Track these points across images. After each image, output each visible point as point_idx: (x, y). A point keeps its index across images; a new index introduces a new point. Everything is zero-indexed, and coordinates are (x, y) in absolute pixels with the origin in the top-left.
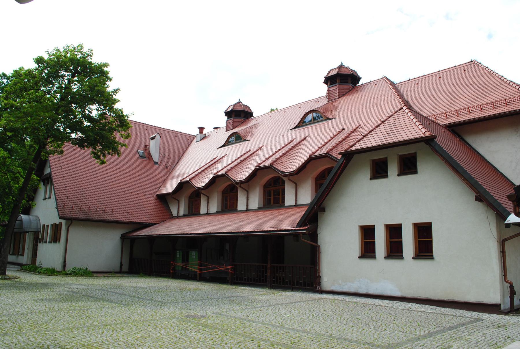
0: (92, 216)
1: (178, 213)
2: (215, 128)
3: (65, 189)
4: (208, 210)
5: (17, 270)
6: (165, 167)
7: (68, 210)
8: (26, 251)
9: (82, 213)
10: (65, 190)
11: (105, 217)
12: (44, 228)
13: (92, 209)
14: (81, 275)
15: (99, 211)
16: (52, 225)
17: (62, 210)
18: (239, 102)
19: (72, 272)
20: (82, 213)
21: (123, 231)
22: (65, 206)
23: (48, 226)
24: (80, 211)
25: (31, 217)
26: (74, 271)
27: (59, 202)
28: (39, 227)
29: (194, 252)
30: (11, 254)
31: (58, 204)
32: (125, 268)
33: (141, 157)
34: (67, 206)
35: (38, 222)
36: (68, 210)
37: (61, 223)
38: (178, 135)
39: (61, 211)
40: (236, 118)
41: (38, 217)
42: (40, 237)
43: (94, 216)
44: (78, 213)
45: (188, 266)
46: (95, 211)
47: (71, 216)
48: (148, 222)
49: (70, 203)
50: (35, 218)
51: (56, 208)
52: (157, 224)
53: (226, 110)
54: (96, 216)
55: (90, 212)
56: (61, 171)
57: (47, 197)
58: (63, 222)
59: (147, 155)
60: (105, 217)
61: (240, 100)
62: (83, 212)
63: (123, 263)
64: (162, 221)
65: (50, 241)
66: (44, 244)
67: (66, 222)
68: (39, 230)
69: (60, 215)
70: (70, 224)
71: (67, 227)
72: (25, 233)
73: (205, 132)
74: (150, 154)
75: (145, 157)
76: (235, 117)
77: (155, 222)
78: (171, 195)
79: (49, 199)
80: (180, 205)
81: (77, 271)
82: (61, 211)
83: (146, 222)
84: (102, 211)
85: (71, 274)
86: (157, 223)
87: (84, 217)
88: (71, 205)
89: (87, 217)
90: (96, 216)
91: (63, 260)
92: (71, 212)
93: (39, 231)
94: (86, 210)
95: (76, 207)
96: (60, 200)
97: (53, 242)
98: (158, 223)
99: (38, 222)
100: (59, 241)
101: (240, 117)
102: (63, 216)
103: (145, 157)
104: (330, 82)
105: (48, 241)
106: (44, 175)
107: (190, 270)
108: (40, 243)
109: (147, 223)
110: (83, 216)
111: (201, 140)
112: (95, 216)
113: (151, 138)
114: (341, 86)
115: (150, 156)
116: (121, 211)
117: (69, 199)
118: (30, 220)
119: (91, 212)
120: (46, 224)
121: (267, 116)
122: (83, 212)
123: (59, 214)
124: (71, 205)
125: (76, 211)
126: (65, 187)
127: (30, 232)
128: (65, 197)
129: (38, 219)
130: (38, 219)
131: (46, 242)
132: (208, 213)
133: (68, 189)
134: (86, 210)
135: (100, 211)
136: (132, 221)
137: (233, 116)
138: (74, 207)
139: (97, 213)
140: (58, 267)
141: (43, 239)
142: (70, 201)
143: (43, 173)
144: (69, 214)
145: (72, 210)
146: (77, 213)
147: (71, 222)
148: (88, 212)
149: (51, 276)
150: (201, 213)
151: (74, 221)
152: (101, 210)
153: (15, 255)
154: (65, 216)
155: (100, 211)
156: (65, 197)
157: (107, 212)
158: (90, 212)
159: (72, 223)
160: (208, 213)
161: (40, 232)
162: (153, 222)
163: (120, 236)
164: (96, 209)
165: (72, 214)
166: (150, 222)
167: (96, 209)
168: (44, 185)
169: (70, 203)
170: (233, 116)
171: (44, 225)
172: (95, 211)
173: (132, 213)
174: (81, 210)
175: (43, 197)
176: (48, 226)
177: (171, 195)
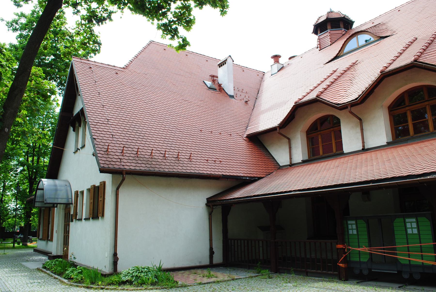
0: (157, 166)
1: (291, 159)
2: (290, 58)
3: (107, 123)
4: (363, 142)
5: (38, 269)
6: (243, 102)
7: (115, 157)
8: (55, 235)
9: (140, 162)
10: (108, 125)
11: (180, 168)
12: (77, 197)
13: (156, 154)
14: (153, 284)
15: (168, 158)
16: (89, 190)
17: (104, 156)
18: (331, 12)
19: (133, 276)
20: (140, 162)
21: (210, 193)
22: (109, 150)
23: (82, 192)
24: (137, 159)
25: (57, 182)
26: (137, 276)
27: (98, 143)
28: (70, 197)
29: (354, 222)
30: (41, 239)
31: (96, 146)
32: (218, 258)
33: (209, 88)
34: (113, 150)
35: (69, 188)
36: (115, 157)
37: (103, 184)
38: (245, 70)
39: (102, 159)
40: (334, 29)
41: (68, 181)
42: (72, 213)
43: (161, 166)
44: (134, 161)
45: (396, 254)
46: (162, 158)
47: (122, 167)
48: (249, 175)
49: (119, 145)
50: (63, 183)
51: (93, 155)
52: (262, 178)
53: (317, 20)
54: (166, 167)
55: (154, 160)
56: (99, 97)
57: (80, 146)
58: (107, 178)
59: (216, 87)
60: (180, 168)
61: (331, 10)
62: (141, 159)
63: (214, 250)
64: (268, 174)
65: (88, 217)
66: (79, 223)
67: (112, 176)
68: (70, 200)
69: (102, 165)
70: (119, 182)
71: (115, 189)
72: (52, 209)
73: (281, 60)
74: (220, 85)
75: (216, 89)
76: (332, 28)
77: (259, 176)
78: (278, 129)
79: (83, 149)
80: (293, 146)
81: (143, 274)
82: (102, 159)
83: (246, 175)
84: (173, 159)
85: (130, 282)
86: (262, 176)
87: (146, 168)
88: (119, 148)
89: (151, 169)
90: (166, 167)
91: (112, 252)
92: (121, 159)
93: (70, 202)
94: (146, 156)
95: (128, 152)
96: (100, 141)
97: (92, 218)
98: (263, 177)
99: (69, 188)
100: (103, 216)
101: (339, 27)
102: (106, 166)
103: (216, 89)
104: (320, 30)
105: (84, 217)
106: (74, 115)
107: (402, 262)
108: (72, 221)
109: (246, 177)
110: (143, 168)
111: (278, 71)
112: (163, 167)
113: (218, 65)
114: (333, 32)
115: (221, 89)
116: (203, 159)
117: (114, 139)
118: (56, 186)
119: (156, 160)
120: (80, 190)
121: (395, 12)
122: (141, 159)
123: (99, 164)
124: (119, 148)
125: (131, 158)
126: (107, 120)
127: (59, 205)
128: (108, 136)
129: (68, 184)
130: (68, 184)
131: (80, 220)
132: (366, 148)
133: (111, 123)
134: (146, 156)
135: (170, 159)
136: (224, 174)
137: (329, 27)
138: (124, 152)
139: (165, 161)
140: (106, 268)
141: (76, 215)
142: (118, 142)
143: (73, 114)
144: (117, 163)
145: (123, 156)
146: (131, 161)
147: (121, 179)
148: (150, 160)
149: (91, 288)
150: (345, 152)
151: (127, 177)
152: (171, 156)
153: (45, 240)
154: (110, 166)
155: (170, 159)
156: (108, 136)
157: (181, 159)
158: (154, 160)
159: (123, 180)
160: (366, 148)
161: (72, 204)
162: (256, 176)
163: (205, 201)
164: (162, 155)
165: (123, 164)
166: (252, 176)
167: (162, 155)
168: (74, 131)
169: (119, 145)
170: (329, 27)
171: (77, 192)
172: (162, 158)
173: (221, 161)
174: (138, 157)
175: (73, 150)
176: (82, 192)
177: (278, 129)
